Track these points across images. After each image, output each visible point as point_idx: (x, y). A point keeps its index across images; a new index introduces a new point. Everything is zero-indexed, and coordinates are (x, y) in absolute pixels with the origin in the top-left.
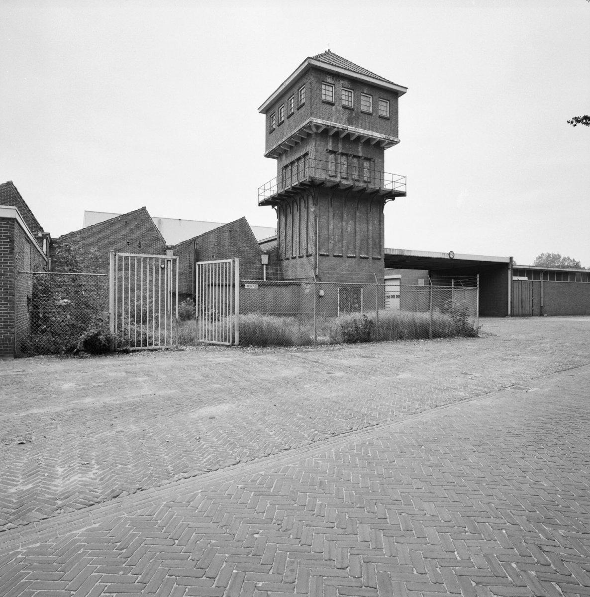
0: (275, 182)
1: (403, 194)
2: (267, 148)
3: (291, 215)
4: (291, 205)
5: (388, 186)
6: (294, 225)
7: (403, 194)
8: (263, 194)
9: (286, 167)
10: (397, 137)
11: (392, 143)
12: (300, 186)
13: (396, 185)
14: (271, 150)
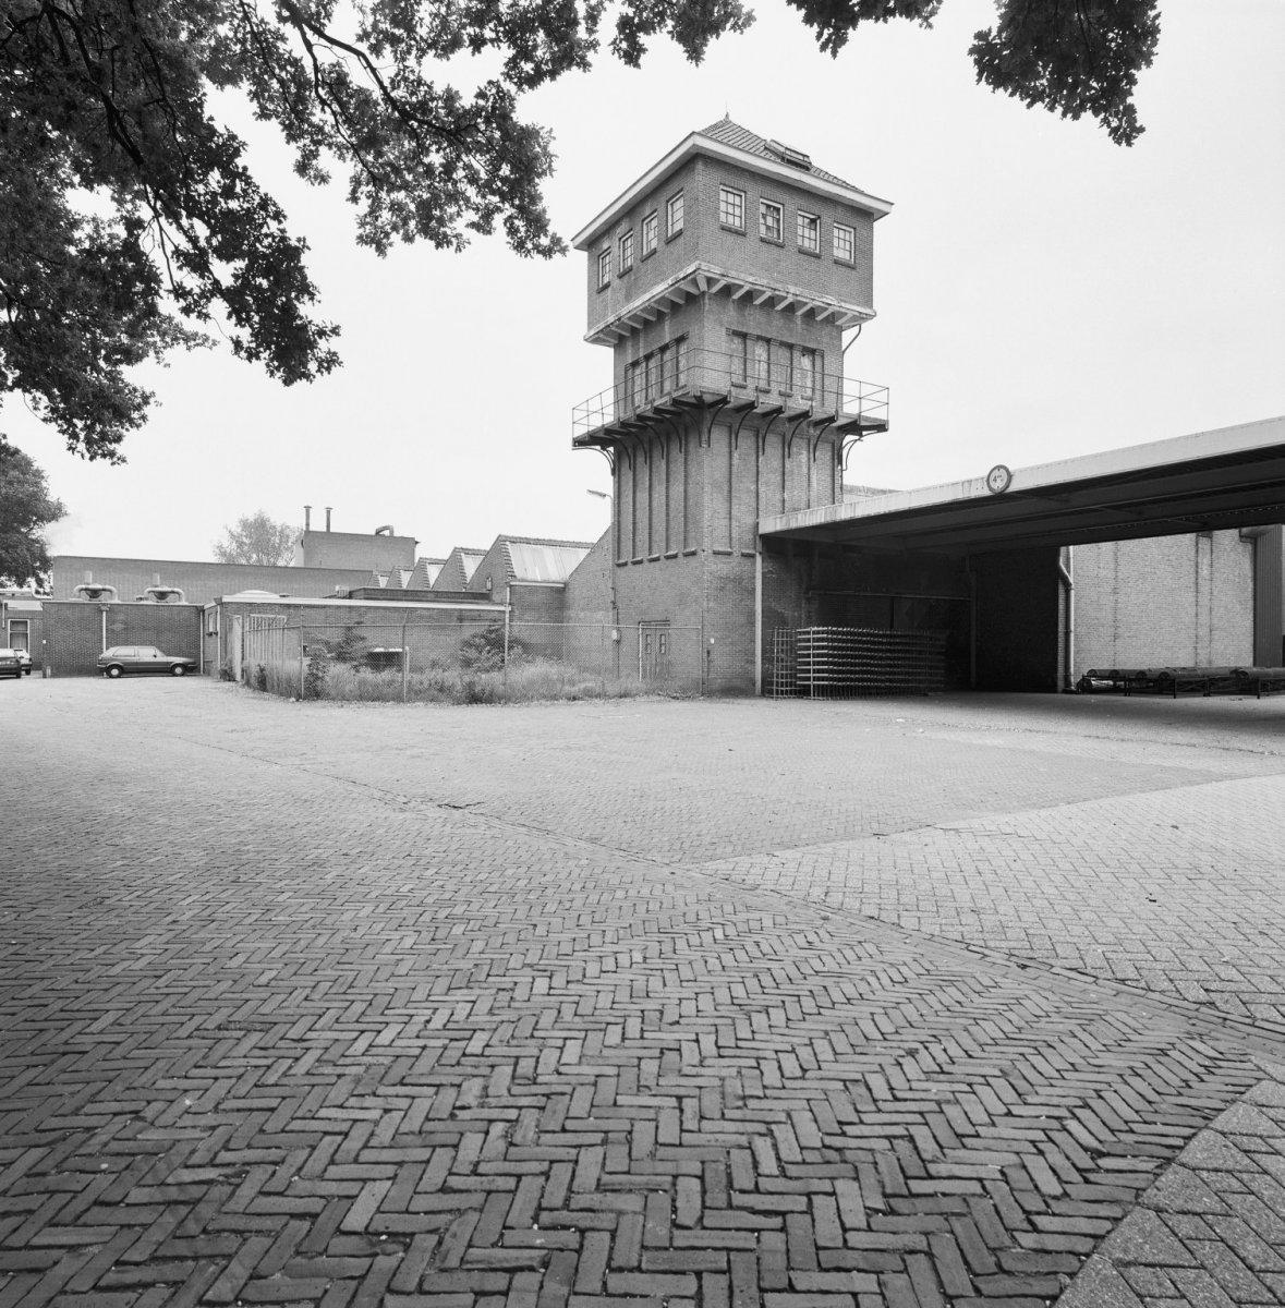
0: (609, 397)
1: (881, 427)
2: (590, 325)
3: (664, 462)
4: (663, 439)
5: (850, 409)
6: (623, 489)
7: (580, 443)
8: (585, 421)
9: (635, 364)
10: (871, 307)
11: (859, 319)
12: (672, 405)
13: (866, 405)
14: (601, 326)
